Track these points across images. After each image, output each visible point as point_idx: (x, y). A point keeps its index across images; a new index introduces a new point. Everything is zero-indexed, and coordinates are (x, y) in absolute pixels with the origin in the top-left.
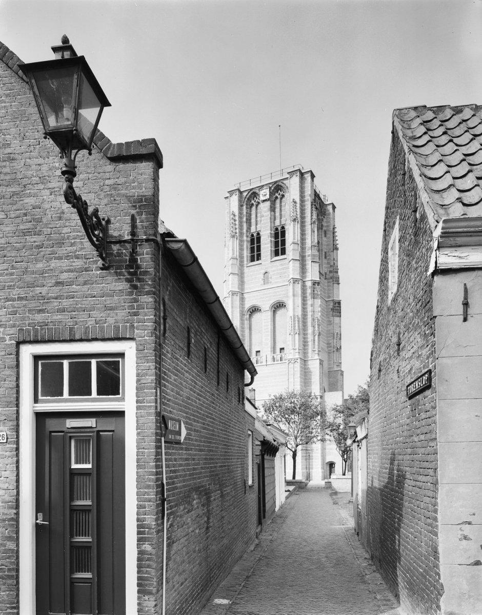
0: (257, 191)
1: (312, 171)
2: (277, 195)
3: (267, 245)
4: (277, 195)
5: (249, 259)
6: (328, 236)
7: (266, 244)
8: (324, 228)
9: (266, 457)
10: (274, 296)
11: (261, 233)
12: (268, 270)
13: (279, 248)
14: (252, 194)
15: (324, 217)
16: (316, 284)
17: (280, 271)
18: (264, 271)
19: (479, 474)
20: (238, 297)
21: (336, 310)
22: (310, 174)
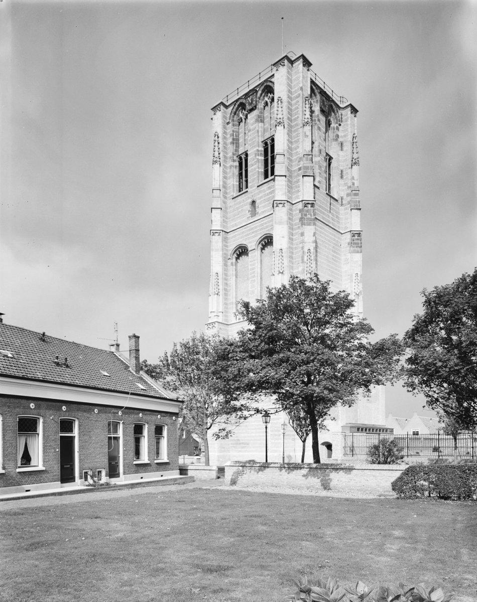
0: (244, 101)
1: (305, 55)
2: (266, 99)
3: (256, 167)
4: (266, 99)
5: (235, 189)
6: (345, 148)
7: (252, 166)
8: (340, 139)
9: (300, 461)
10: (261, 229)
11: (249, 153)
12: (255, 199)
13: (269, 171)
14: (239, 106)
15: (340, 125)
16: (309, 206)
17: (268, 197)
18: (250, 200)
19: (310, 294)
20: (220, 237)
21: (355, 244)
22: (301, 60)
